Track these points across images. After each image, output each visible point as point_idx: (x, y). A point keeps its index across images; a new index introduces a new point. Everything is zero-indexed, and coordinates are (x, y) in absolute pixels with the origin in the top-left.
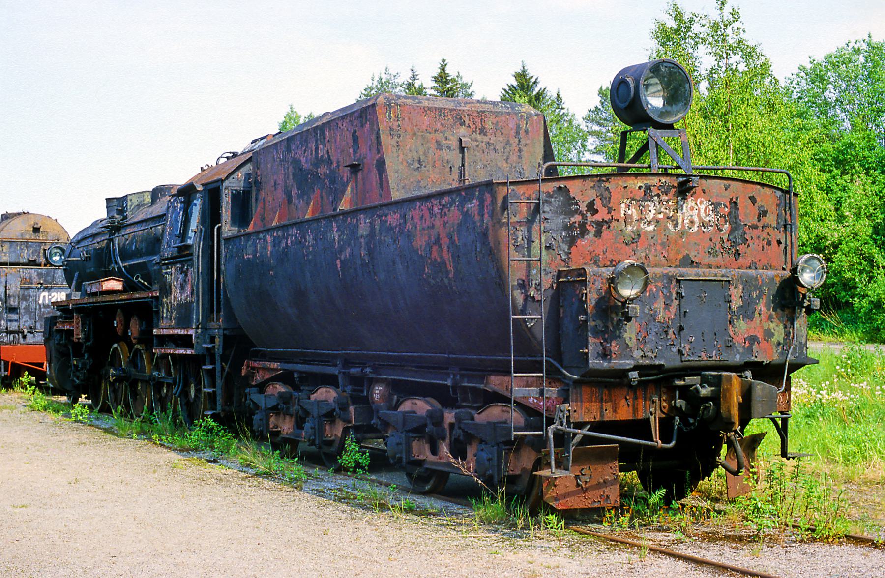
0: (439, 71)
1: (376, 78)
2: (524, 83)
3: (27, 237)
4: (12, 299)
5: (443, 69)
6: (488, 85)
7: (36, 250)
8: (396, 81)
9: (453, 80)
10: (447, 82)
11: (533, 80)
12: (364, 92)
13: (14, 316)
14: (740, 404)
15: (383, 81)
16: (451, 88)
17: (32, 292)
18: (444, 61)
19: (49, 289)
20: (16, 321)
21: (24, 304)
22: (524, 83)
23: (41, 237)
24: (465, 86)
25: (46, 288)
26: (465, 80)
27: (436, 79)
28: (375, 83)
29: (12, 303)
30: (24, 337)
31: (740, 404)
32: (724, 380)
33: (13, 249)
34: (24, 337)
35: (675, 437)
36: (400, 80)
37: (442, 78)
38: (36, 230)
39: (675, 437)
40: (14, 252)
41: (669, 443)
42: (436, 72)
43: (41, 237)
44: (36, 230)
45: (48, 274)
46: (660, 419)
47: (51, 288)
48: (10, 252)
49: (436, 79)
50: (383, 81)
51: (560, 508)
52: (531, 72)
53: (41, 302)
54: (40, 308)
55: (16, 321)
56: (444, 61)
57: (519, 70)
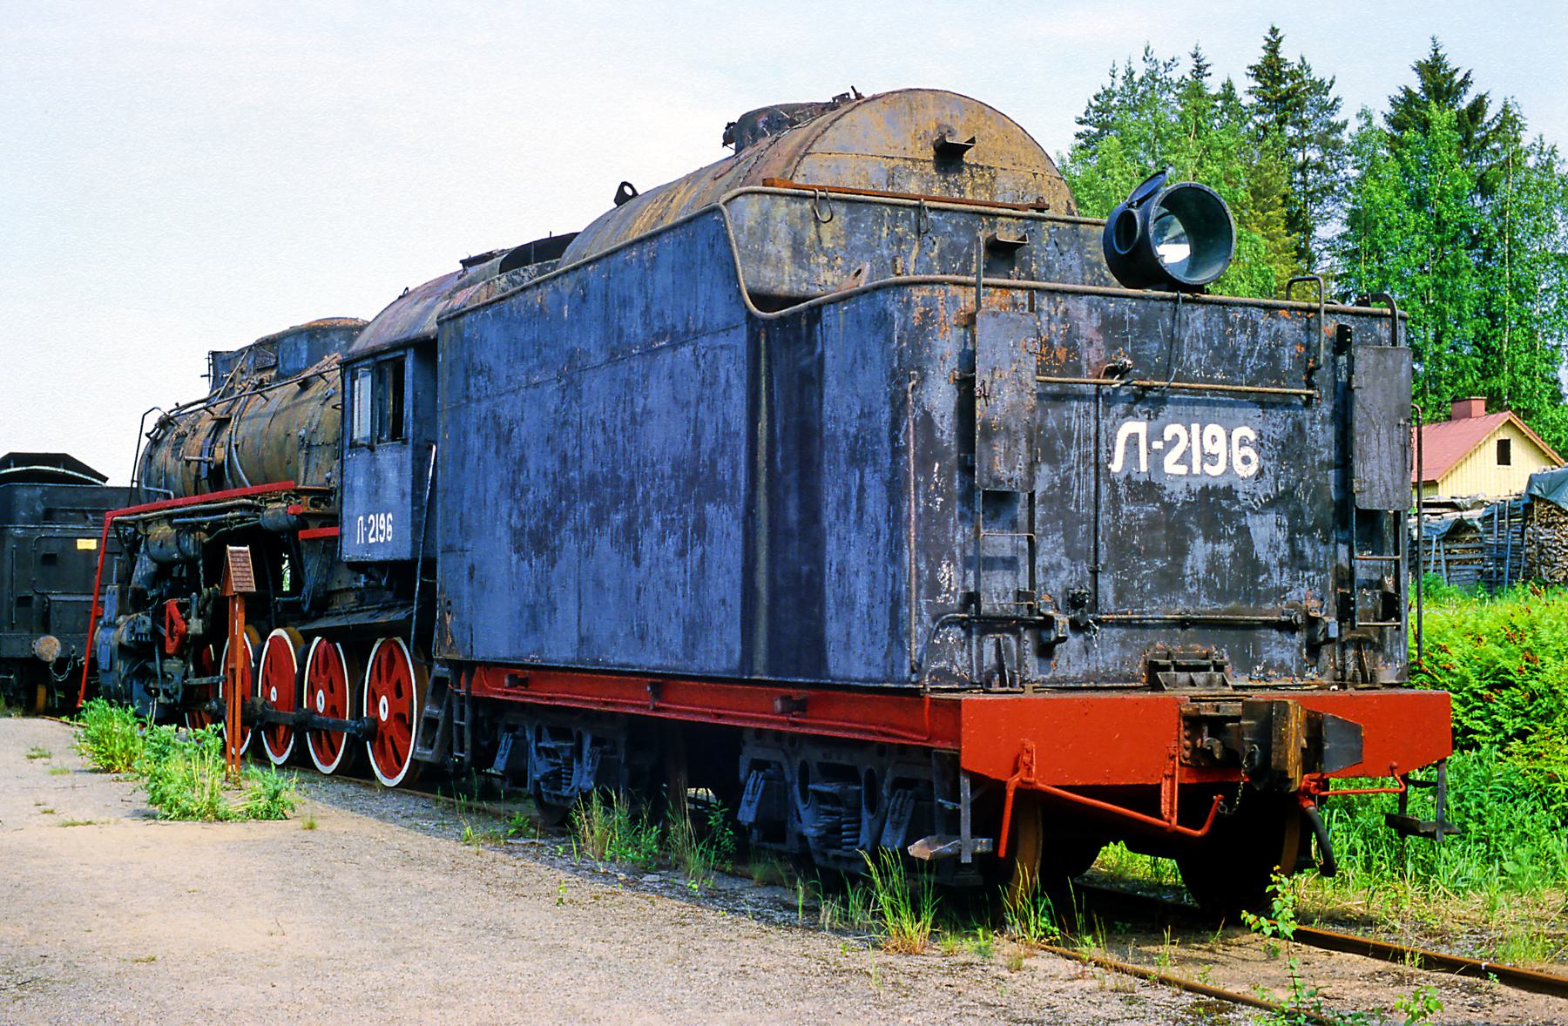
0: (1264, 53)
1: (1121, 73)
2: (1438, 81)
3: (913, 187)
4: (1000, 447)
5: (1273, 47)
6: (1365, 86)
7: (954, 249)
8: (1168, 75)
9: (1293, 75)
10: (1280, 80)
11: (1458, 78)
12: (1095, 103)
13: (1000, 542)
14: (1303, 749)
15: (1136, 78)
16: (1295, 90)
17: (1077, 416)
18: (1274, 31)
19: (1147, 400)
20: (1010, 564)
21: (1045, 478)
22: (1438, 81)
23: (970, 190)
24: (1320, 87)
25: (1140, 396)
26: (1317, 74)
27: (1257, 72)
28: (1119, 83)
29: (1001, 470)
30: (1046, 651)
31: (1303, 749)
32: (747, 736)
33: (859, 239)
34: (1046, 651)
35: (1208, 822)
36: (1175, 75)
37: (1270, 70)
38: (949, 156)
39: (1208, 822)
40: (869, 249)
41: (1198, 829)
42: (1257, 56)
43: (970, 190)
44: (949, 156)
45: (1146, 326)
46: (1180, 785)
47: (1161, 401)
48: (850, 250)
49: (1257, 72)
50: (1136, 78)
51: (1282, 997)
52: (1457, 60)
53: (1116, 467)
54: (1115, 501)
55: (1010, 564)
56: (1274, 31)
57: (1425, 56)
